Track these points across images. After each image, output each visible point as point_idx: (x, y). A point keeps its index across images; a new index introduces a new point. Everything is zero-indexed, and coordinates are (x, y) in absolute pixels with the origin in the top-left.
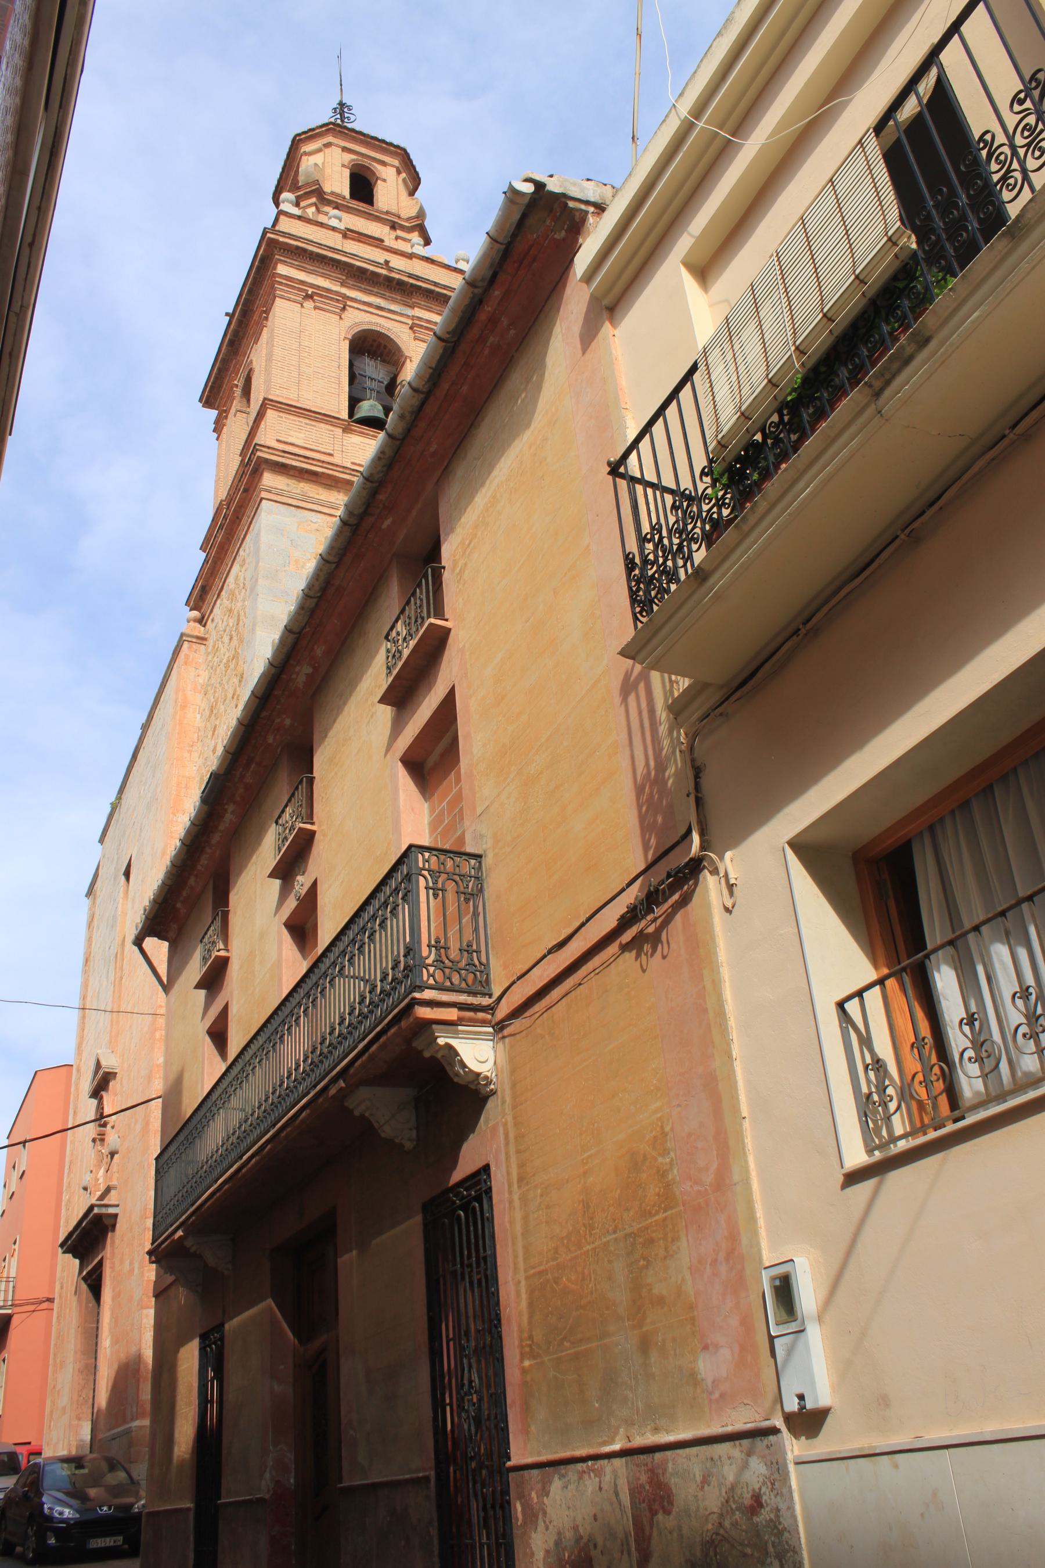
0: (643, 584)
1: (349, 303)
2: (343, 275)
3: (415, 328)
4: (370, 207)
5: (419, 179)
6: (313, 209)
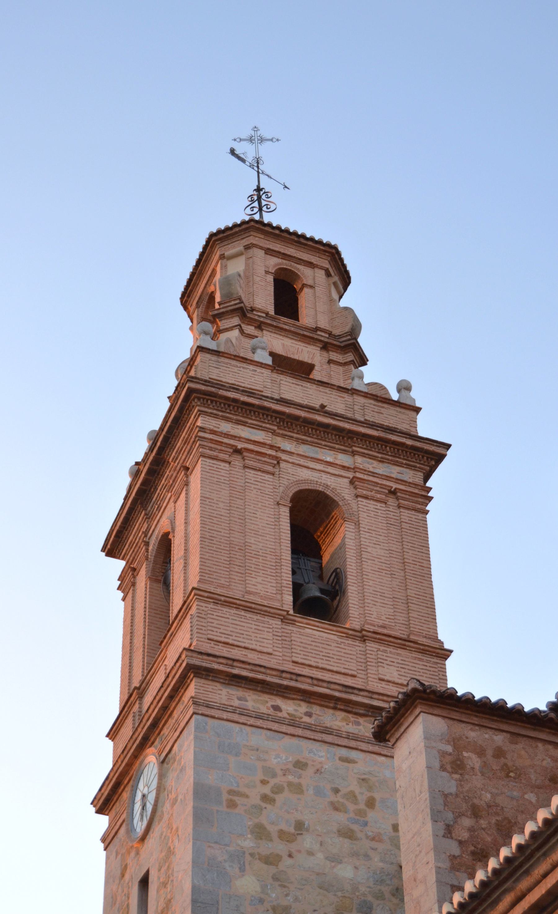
1: (284, 456)
2: (274, 425)
3: (357, 483)
4: (296, 323)
5: (349, 278)
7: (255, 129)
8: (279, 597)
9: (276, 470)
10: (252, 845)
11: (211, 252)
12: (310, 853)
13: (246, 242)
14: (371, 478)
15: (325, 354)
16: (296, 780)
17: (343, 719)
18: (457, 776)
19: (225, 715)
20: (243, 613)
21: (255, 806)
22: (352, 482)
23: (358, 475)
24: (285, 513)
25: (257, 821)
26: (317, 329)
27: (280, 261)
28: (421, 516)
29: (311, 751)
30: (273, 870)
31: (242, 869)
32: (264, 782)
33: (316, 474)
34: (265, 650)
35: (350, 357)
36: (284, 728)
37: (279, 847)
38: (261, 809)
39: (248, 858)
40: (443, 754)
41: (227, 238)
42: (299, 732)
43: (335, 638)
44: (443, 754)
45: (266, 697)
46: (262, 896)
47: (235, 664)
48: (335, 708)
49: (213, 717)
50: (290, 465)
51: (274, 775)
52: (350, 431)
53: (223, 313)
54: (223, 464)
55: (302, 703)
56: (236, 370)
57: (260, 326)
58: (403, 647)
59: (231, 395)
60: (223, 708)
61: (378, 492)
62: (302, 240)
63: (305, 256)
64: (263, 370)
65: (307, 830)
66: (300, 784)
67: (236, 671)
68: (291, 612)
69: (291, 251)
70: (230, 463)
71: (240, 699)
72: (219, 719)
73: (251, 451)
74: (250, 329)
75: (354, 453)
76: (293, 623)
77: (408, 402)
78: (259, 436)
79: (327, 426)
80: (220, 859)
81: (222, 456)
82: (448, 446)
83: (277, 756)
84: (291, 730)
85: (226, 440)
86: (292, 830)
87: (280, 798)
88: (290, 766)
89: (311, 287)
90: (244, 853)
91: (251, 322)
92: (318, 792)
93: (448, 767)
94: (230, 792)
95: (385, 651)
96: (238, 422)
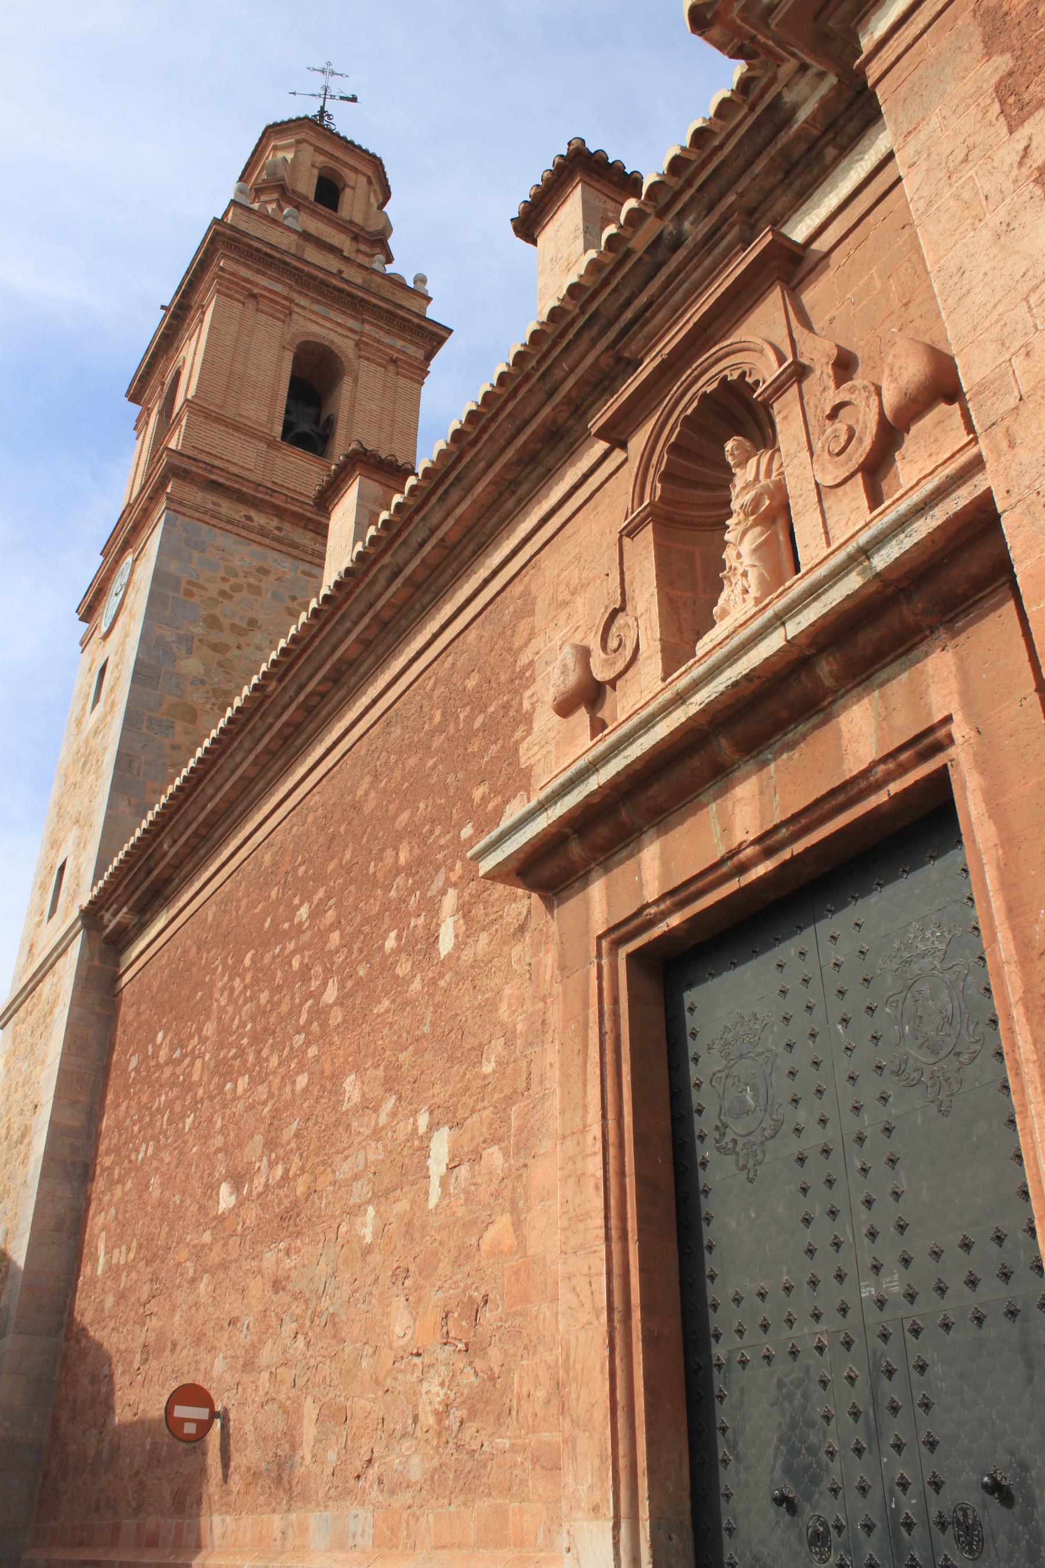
0: (342, 937)
1: (296, 309)
4: (334, 213)
5: (390, 193)
6: (274, 206)
8: (269, 425)
9: (287, 320)
10: (202, 632)
11: (267, 144)
13: (298, 137)
15: (354, 244)
16: (257, 583)
17: (312, 539)
19: (196, 515)
20: (231, 431)
21: (212, 599)
22: (357, 345)
23: (364, 339)
25: (211, 612)
26: (351, 222)
28: (416, 385)
29: (275, 561)
30: (219, 657)
31: (189, 652)
33: (326, 332)
34: (247, 466)
36: (253, 536)
37: (230, 639)
38: (217, 602)
39: (196, 642)
41: (282, 131)
42: (267, 541)
43: (317, 470)
45: (240, 507)
46: (205, 678)
47: (214, 470)
48: (305, 528)
49: (184, 514)
50: (301, 318)
51: (236, 575)
52: (362, 300)
53: (264, 188)
54: (236, 303)
55: (275, 518)
56: (265, 228)
60: (196, 508)
61: (379, 357)
63: (352, 162)
64: (291, 235)
65: (259, 628)
66: (259, 587)
67: (213, 477)
68: (279, 439)
69: (338, 154)
70: (244, 304)
71: (214, 504)
72: (189, 517)
73: (266, 298)
75: (363, 321)
78: (278, 288)
79: (342, 291)
80: (168, 639)
81: (237, 296)
82: (450, 331)
83: (241, 560)
84: (259, 538)
85: (243, 283)
86: (244, 625)
87: (238, 596)
88: (253, 570)
89: (353, 188)
90: (193, 638)
91: (290, 202)
92: (276, 596)
94: (189, 583)
96: (258, 272)
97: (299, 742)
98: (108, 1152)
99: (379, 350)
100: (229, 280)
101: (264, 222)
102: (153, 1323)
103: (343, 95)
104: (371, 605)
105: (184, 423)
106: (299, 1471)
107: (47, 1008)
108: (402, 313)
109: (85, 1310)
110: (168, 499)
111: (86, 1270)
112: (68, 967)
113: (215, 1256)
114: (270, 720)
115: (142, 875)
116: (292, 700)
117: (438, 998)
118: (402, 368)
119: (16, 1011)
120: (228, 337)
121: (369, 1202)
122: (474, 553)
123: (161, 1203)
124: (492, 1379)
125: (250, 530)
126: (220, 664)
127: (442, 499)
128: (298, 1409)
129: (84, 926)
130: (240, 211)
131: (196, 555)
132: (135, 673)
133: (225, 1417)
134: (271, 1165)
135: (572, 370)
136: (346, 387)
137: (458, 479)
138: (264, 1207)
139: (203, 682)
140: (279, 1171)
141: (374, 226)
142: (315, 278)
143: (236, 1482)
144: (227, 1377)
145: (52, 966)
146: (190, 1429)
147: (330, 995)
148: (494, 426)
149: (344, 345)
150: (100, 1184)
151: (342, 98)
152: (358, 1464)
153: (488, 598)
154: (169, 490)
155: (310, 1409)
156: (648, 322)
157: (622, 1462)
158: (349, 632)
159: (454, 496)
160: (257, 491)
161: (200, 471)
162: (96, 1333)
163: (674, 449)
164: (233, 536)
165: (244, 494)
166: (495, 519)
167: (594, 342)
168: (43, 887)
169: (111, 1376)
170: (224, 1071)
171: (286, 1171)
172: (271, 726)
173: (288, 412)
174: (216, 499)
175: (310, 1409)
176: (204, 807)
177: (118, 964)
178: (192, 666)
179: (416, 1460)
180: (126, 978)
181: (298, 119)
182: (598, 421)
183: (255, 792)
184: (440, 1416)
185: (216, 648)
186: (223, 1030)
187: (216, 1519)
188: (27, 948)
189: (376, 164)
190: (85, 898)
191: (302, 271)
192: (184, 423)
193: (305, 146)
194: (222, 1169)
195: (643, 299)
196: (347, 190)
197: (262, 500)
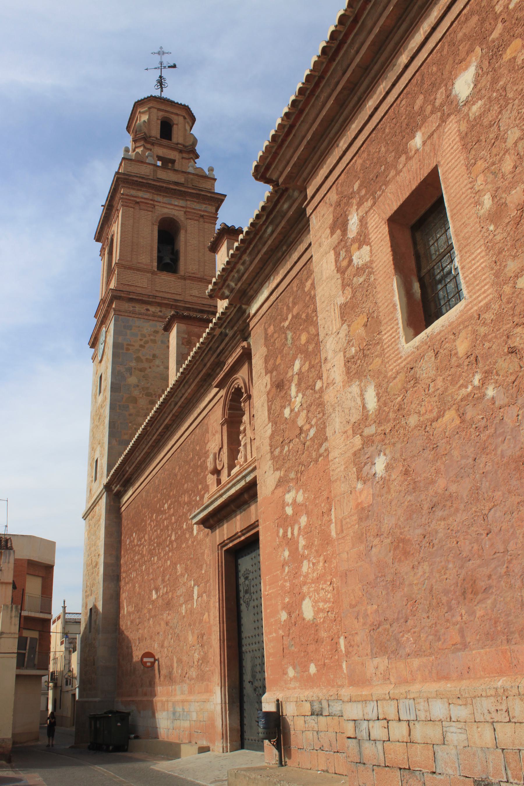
4: (170, 141)
7: (161, 48)
12: (158, 366)
13: (149, 106)
14: (193, 211)
15: (181, 154)
16: (154, 338)
18: (188, 347)
19: (126, 314)
21: (136, 350)
22: (185, 212)
24: (156, 228)
26: (178, 144)
27: (163, 113)
30: (143, 374)
31: (131, 374)
32: (141, 340)
33: (170, 210)
35: (191, 155)
37: (146, 365)
40: (183, 338)
41: (142, 104)
42: (156, 319)
43: (173, 279)
44: (183, 338)
49: (121, 315)
51: (145, 337)
52: (184, 191)
56: (138, 167)
57: (153, 144)
58: (201, 281)
59: (135, 179)
60: (126, 311)
62: (173, 104)
65: (157, 357)
67: (131, 297)
68: (156, 270)
69: (169, 109)
70: (134, 208)
71: (133, 307)
74: (149, 146)
75: (187, 200)
76: (156, 274)
77: (212, 176)
78: (147, 195)
82: (225, 196)
83: (147, 329)
85: (132, 198)
86: (151, 358)
87: (147, 346)
89: (177, 124)
93: (185, 344)
94: (128, 345)
95: (193, 284)
96: (138, 190)
97: (161, 444)
98: (124, 572)
99: (195, 213)
100: (126, 199)
101: (138, 164)
102: (140, 631)
103: (169, 65)
104: (171, 411)
105: (116, 272)
106: (174, 675)
107: (98, 518)
108: (203, 193)
109: (125, 624)
110: (114, 310)
111: (122, 612)
112: (103, 502)
113: (153, 613)
114: (150, 437)
115: (122, 476)
116: (156, 433)
117: (194, 548)
118: (206, 219)
119: (88, 515)
120: (129, 226)
121: (183, 603)
122: (196, 401)
123: (139, 593)
124: (206, 654)
125: (149, 315)
126: (144, 377)
127: (184, 386)
128: (173, 659)
129: (106, 491)
130: (127, 161)
131: (128, 332)
132: (111, 388)
133: (158, 660)
134: (164, 587)
135: (209, 360)
136: (182, 236)
137: (187, 382)
138: (163, 599)
139: (138, 386)
140: (165, 590)
141: (189, 143)
142: (163, 187)
143: (162, 678)
144: (158, 649)
145: (98, 502)
146: (149, 664)
147: (173, 538)
148: (192, 371)
149: (179, 215)
150: (122, 583)
151: (169, 67)
152: (184, 674)
153: (200, 421)
154: (114, 306)
155: (175, 660)
156: (224, 354)
157: (223, 674)
158: (167, 417)
159: (187, 387)
160: (149, 298)
161: (125, 295)
162: (127, 633)
163: (231, 400)
164: (142, 320)
165: (144, 300)
166: (199, 394)
167: (212, 355)
168: (91, 465)
169: (131, 647)
170: (151, 553)
171: (167, 590)
172: (151, 439)
173: (159, 251)
174: (133, 305)
175: (175, 660)
176: (136, 459)
177: (120, 503)
178: (132, 380)
179: (194, 673)
180: (123, 509)
181: (148, 97)
182: (215, 383)
183: (151, 456)
184: (198, 662)
185: (141, 370)
186: (150, 539)
187: (159, 688)
188: (89, 490)
189: (186, 109)
190: (105, 481)
191: (157, 185)
192: (116, 272)
193: (152, 110)
194: (153, 586)
195: (221, 348)
196: (175, 126)
197: (152, 301)
